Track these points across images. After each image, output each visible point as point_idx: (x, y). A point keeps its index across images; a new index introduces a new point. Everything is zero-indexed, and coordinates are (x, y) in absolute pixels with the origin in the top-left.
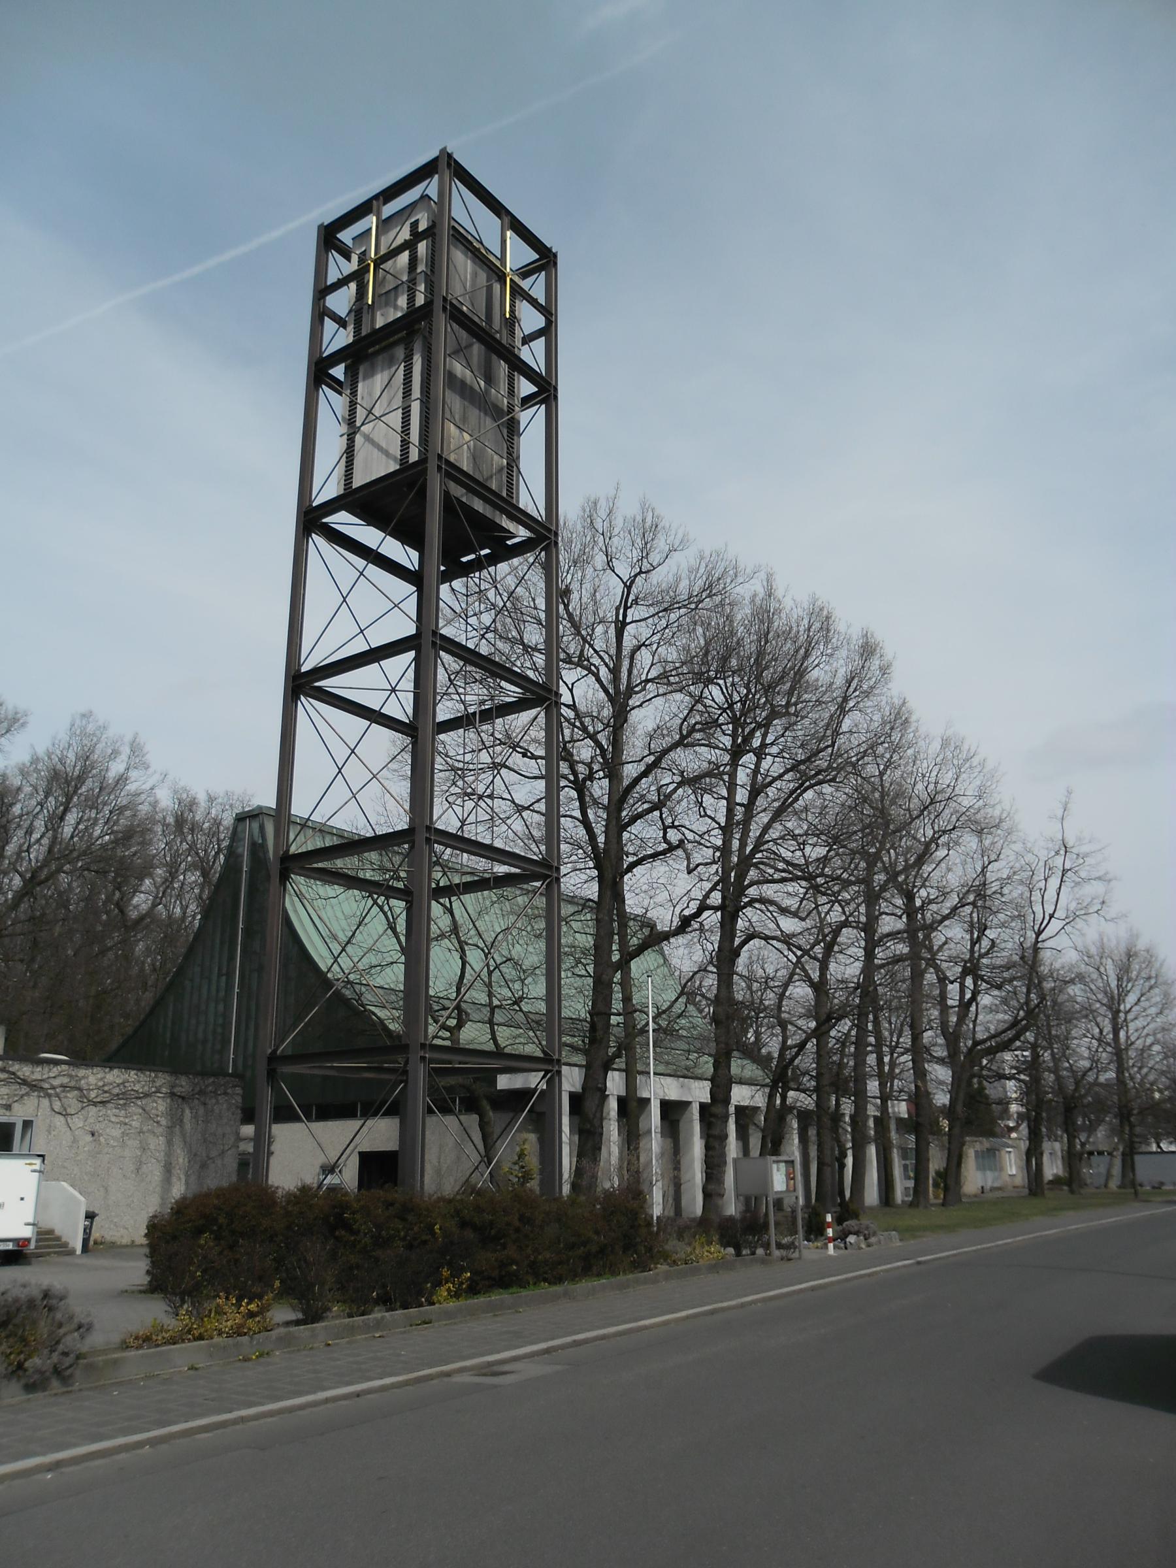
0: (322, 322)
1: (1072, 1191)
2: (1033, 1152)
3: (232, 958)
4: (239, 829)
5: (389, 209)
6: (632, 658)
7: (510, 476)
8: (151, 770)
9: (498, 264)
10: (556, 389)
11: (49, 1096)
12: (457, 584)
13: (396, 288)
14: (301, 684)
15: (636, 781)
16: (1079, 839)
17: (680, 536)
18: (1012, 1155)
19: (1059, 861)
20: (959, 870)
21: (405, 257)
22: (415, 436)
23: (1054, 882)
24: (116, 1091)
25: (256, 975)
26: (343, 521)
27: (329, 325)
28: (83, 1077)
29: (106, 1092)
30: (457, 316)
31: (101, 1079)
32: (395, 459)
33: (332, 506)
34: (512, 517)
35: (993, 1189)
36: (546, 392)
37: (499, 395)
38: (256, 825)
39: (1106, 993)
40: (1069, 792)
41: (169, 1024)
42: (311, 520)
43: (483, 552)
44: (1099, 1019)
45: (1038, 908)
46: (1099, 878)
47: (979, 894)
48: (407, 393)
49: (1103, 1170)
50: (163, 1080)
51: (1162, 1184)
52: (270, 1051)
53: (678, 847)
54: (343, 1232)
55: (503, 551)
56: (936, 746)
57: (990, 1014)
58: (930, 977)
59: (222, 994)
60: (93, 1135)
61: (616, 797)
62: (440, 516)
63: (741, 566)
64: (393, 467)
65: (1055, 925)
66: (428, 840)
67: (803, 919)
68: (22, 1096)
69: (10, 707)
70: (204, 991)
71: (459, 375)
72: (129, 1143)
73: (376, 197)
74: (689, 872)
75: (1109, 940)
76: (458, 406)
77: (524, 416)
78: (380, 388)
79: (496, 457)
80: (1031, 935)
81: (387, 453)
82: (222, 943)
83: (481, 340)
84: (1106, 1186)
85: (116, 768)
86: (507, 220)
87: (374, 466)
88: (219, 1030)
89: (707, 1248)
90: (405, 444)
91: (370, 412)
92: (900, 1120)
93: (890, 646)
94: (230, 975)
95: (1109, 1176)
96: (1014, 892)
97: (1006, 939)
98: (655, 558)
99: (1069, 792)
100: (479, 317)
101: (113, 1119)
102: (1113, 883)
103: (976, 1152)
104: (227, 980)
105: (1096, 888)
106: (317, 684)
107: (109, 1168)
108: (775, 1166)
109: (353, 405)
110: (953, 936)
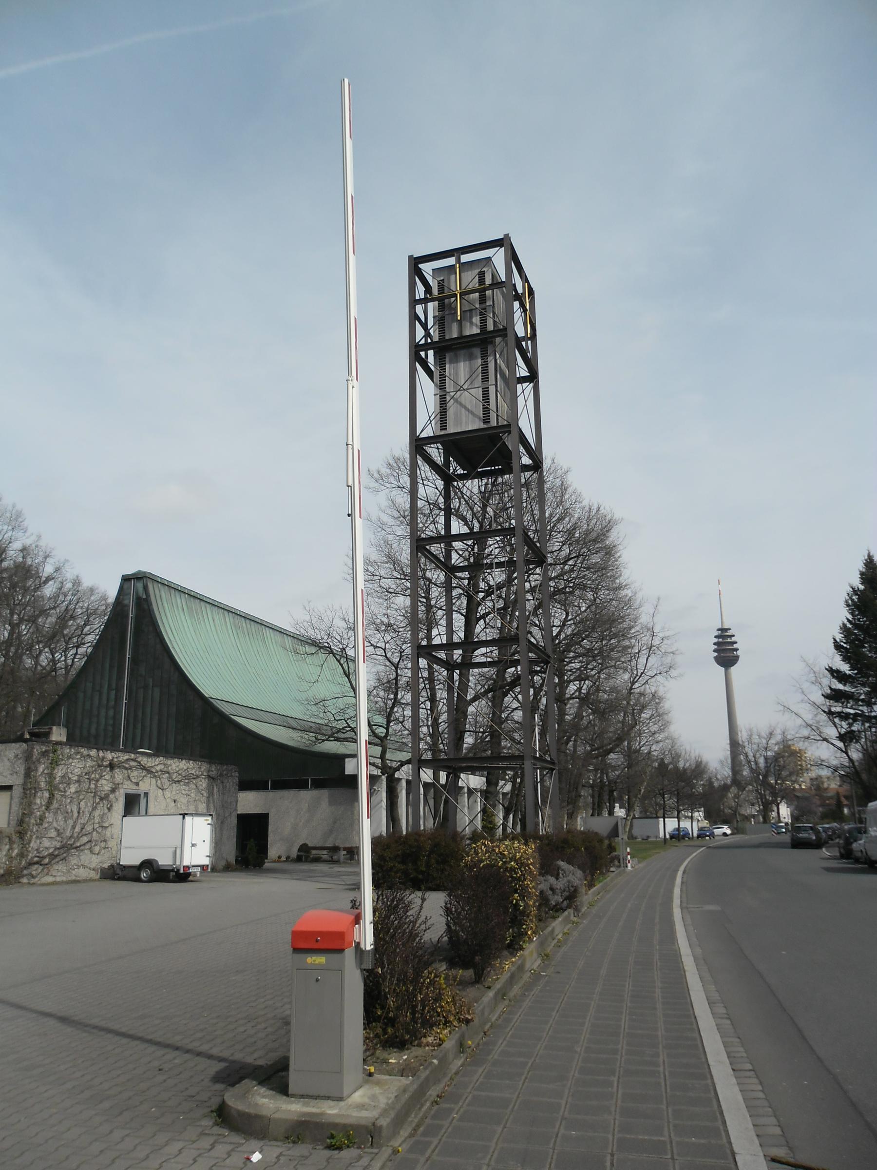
3: (120, 677)
4: (126, 586)
5: (465, 258)
8: (28, 534)
11: (155, 777)
24: (184, 774)
25: (142, 690)
28: (170, 765)
32: (480, 418)
38: (140, 585)
50: (205, 766)
51: (648, 837)
59: (112, 703)
64: (478, 425)
70: (96, 701)
78: (461, 370)
82: (111, 667)
88: (110, 728)
90: (486, 410)
94: (119, 690)
104: (116, 695)
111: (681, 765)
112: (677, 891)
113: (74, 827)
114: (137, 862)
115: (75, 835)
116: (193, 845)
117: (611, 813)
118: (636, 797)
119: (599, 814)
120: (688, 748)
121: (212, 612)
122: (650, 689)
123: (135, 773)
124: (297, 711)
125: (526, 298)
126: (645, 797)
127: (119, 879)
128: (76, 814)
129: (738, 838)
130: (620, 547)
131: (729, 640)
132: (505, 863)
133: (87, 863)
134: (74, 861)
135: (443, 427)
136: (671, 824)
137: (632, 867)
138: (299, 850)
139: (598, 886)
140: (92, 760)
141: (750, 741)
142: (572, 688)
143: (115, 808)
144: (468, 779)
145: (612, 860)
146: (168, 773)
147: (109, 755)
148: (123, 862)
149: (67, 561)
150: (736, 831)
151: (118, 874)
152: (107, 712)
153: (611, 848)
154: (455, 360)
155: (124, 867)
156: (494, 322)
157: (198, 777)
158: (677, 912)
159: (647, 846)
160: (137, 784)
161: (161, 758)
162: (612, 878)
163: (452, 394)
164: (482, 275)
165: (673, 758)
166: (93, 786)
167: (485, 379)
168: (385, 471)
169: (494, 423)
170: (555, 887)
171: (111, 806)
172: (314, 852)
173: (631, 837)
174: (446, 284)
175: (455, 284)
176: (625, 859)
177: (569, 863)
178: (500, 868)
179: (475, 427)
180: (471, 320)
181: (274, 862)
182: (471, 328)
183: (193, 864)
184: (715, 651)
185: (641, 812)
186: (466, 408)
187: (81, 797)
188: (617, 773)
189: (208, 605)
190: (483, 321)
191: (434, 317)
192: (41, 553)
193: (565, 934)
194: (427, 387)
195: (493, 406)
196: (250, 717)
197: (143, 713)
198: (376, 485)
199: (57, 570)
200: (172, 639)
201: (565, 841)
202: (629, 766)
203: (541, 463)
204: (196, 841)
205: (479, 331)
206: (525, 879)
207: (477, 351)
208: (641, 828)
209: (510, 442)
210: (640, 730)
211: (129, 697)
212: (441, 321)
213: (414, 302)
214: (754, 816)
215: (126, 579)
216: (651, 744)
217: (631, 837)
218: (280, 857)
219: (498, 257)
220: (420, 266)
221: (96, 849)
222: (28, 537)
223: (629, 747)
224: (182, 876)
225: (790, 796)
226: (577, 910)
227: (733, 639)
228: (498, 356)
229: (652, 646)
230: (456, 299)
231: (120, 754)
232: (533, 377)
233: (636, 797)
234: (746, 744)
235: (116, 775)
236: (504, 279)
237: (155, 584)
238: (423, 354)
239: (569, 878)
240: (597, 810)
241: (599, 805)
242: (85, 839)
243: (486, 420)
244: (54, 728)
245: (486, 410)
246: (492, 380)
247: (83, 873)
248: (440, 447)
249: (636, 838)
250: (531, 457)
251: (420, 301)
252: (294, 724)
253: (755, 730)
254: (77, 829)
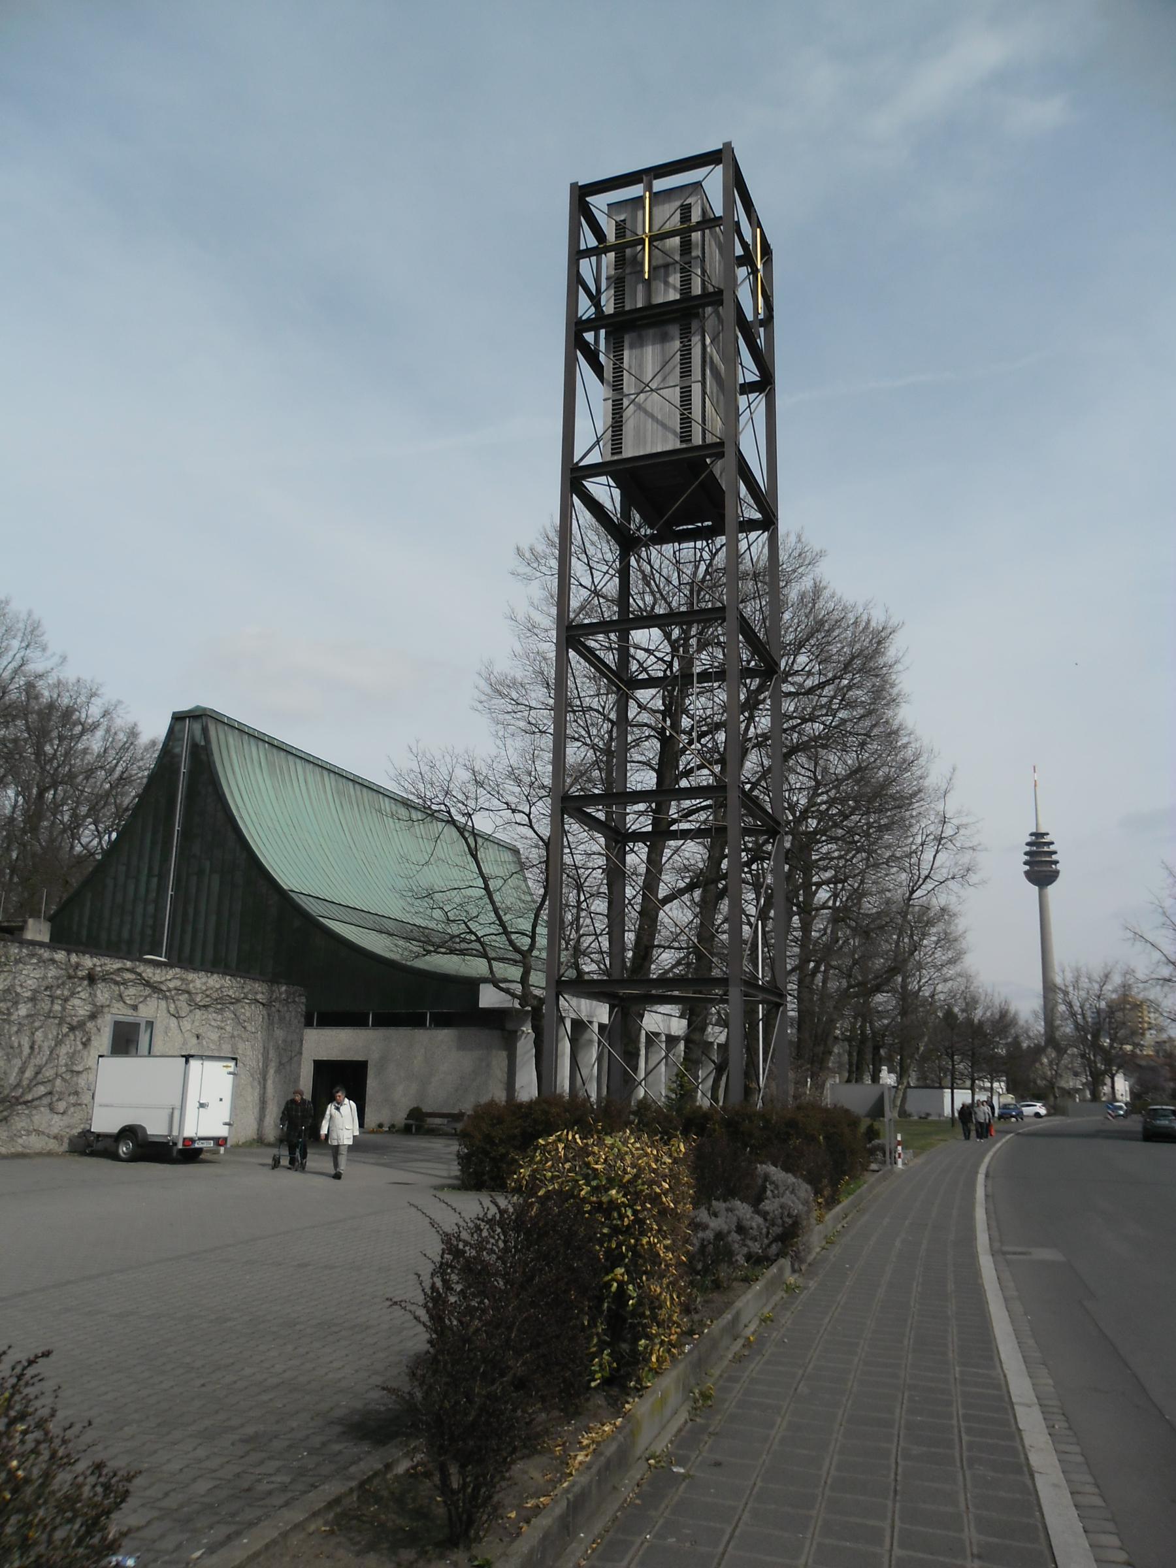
3: (165, 859)
4: (177, 728)
5: (660, 185)
8: (49, 653)
11: (166, 998)
12: (668, 549)
24: (215, 995)
25: (195, 877)
28: (192, 981)
29: (207, 996)
31: (205, 983)
32: (674, 432)
33: (595, 470)
38: (197, 727)
41: (86, 921)
43: (706, 524)
50: (259, 989)
51: (928, 1115)
59: (153, 895)
68: (146, 997)
69: (900, 718)
78: (647, 359)
88: (149, 932)
90: (686, 421)
94: (162, 877)
101: (213, 1023)
111: (978, 1014)
112: (980, 1214)
113: (22, 1071)
114: (114, 1129)
115: (25, 1083)
116: (202, 1105)
117: (875, 1078)
118: (912, 1057)
119: (859, 1080)
120: (989, 991)
121: (304, 772)
122: (941, 900)
123: (132, 991)
124: (394, 907)
125: (757, 257)
126: (924, 1058)
127: (93, 1154)
128: (26, 1051)
129: (1057, 1121)
130: (898, 667)
131: (1046, 849)
132: (595, 1190)
133: (46, 1127)
134: (19, 1123)
135: (617, 447)
136: (963, 1097)
137: (904, 1164)
138: (409, 1116)
139: (845, 1202)
140: (58, 967)
141: (1076, 985)
142: (823, 895)
143: (95, 1043)
144: (579, 1006)
145: (872, 1152)
146: (188, 992)
147: (88, 962)
148: (96, 1128)
149: (120, 702)
150: (1053, 1111)
151: (92, 1146)
152: (145, 909)
153: (872, 1134)
154: (639, 343)
155: (99, 1136)
156: (703, 282)
157: (238, 1001)
158: (986, 1263)
159: (922, 1131)
160: (135, 1008)
161: (178, 970)
162: (871, 1187)
163: (633, 397)
164: (686, 210)
165: (967, 1004)
166: (57, 1008)
167: (686, 372)
168: (541, 548)
169: (697, 440)
170: (746, 1223)
171: (89, 1040)
172: (430, 1120)
173: (903, 1113)
174: (628, 225)
175: (644, 225)
176: (893, 1151)
177: (787, 1169)
178: (584, 1200)
179: (669, 447)
180: (667, 282)
181: (373, 1132)
182: (666, 291)
183: (201, 1134)
184: (1025, 863)
185: (918, 1079)
186: (652, 417)
187: (37, 1024)
188: (886, 1022)
189: (298, 761)
190: (686, 282)
191: (607, 279)
192: (84, 691)
193: (763, 1320)
194: (593, 393)
195: (696, 414)
196: (348, 920)
197: (196, 913)
198: (528, 570)
199: (105, 714)
200: (240, 804)
201: (792, 1124)
202: (904, 1013)
203: (775, 516)
204: (208, 1098)
205: (678, 297)
206: (643, 1233)
207: (674, 330)
208: (917, 1102)
209: (722, 470)
210: (919, 962)
211: (177, 887)
212: (619, 283)
213: (577, 254)
214: (1077, 1091)
215: (178, 718)
216: (935, 985)
217: (903, 1113)
218: (380, 1126)
219: (713, 179)
220: (588, 199)
221: (61, 1106)
222: (47, 659)
223: (904, 985)
224: (189, 1154)
225: (1129, 1065)
226: (798, 1258)
227: (1052, 848)
228: (708, 341)
229: (942, 838)
230: (644, 248)
231: (107, 960)
232: (765, 384)
233: (912, 1057)
234: (1071, 989)
235: (99, 993)
236: (719, 212)
237: (220, 727)
238: (589, 336)
239: (782, 1200)
240: (854, 1074)
241: (858, 1068)
242: (42, 1090)
243: (685, 436)
244: (31, 921)
245: (686, 421)
246: (696, 374)
247: (36, 1143)
248: (612, 483)
249: (910, 1115)
250: (761, 509)
251: (588, 253)
252: (390, 926)
253: (1084, 970)
254: (29, 1074)
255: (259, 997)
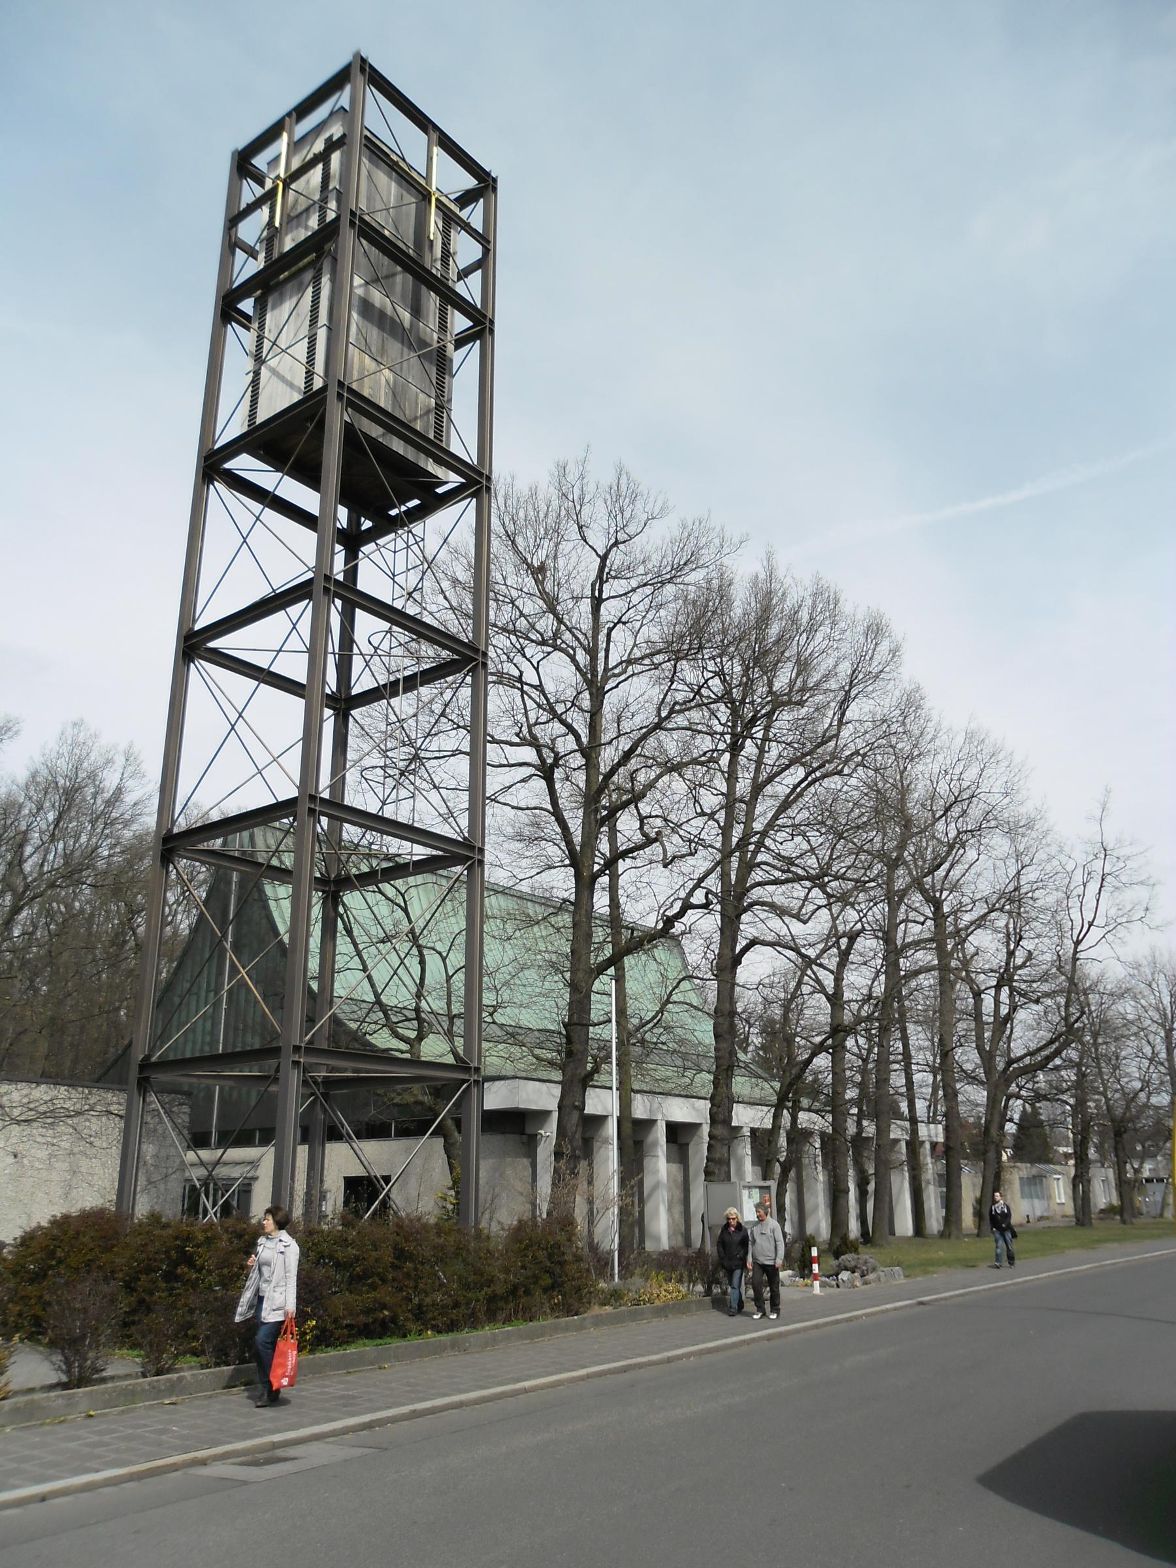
0: (233, 254)
1: (1124, 1222)
2: (1081, 1181)
6: (609, 635)
7: (439, 418)
9: (423, 182)
10: (492, 322)
13: (307, 210)
14: (194, 645)
15: (613, 771)
16: (1118, 841)
17: (659, 503)
18: (1061, 1182)
19: (1097, 865)
20: (989, 874)
21: (316, 174)
22: (319, 367)
23: (1093, 887)
24: (43, 1109)
26: (244, 464)
27: (240, 255)
29: (31, 1110)
30: (369, 232)
34: (439, 461)
35: (1041, 1218)
36: (482, 327)
37: (429, 329)
39: (1158, 1010)
40: (1108, 791)
42: (212, 466)
44: (1151, 1037)
45: (1076, 916)
46: (1142, 883)
47: (1012, 900)
48: (314, 320)
49: (1159, 1198)
52: (141, 1057)
53: (655, 840)
54: (186, 1270)
55: (432, 502)
56: (960, 739)
57: (1028, 1031)
58: (962, 989)
60: (15, 1156)
61: (595, 787)
62: (365, 466)
63: (727, 535)
64: (297, 397)
65: (1095, 934)
66: (312, 811)
67: (805, 922)
71: (377, 304)
72: (57, 1165)
73: (289, 114)
74: (665, 866)
75: (1161, 955)
76: (375, 337)
77: (457, 356)
78: (288, 319)
79: (422, 396)
80: (1069, 944)
81: (291, 385)
83: (407, 268)
84: (1161, 1215)
85: (110, 780)
86: (435, 136)
87: (278, 398)
89: (665, 1286)
90: (310, 375)
91: (274, 343)
92: (934, 1145)
93: (899, 627)
95: (1164, 1204)
96: (1047, 898)
97: (1041, 946)
98: (631, 529)
99: (1108, 791)
100: (407, 241)
101: (39, 1139)
102: (1157, 888)
103: (1021, 1179)
105: (1141, 894)
106: (211, 645)
107: (33, 1193)
108: (745, 1193)
109: (260, 339)
110: (986, 946)
255: (114, 1108)
